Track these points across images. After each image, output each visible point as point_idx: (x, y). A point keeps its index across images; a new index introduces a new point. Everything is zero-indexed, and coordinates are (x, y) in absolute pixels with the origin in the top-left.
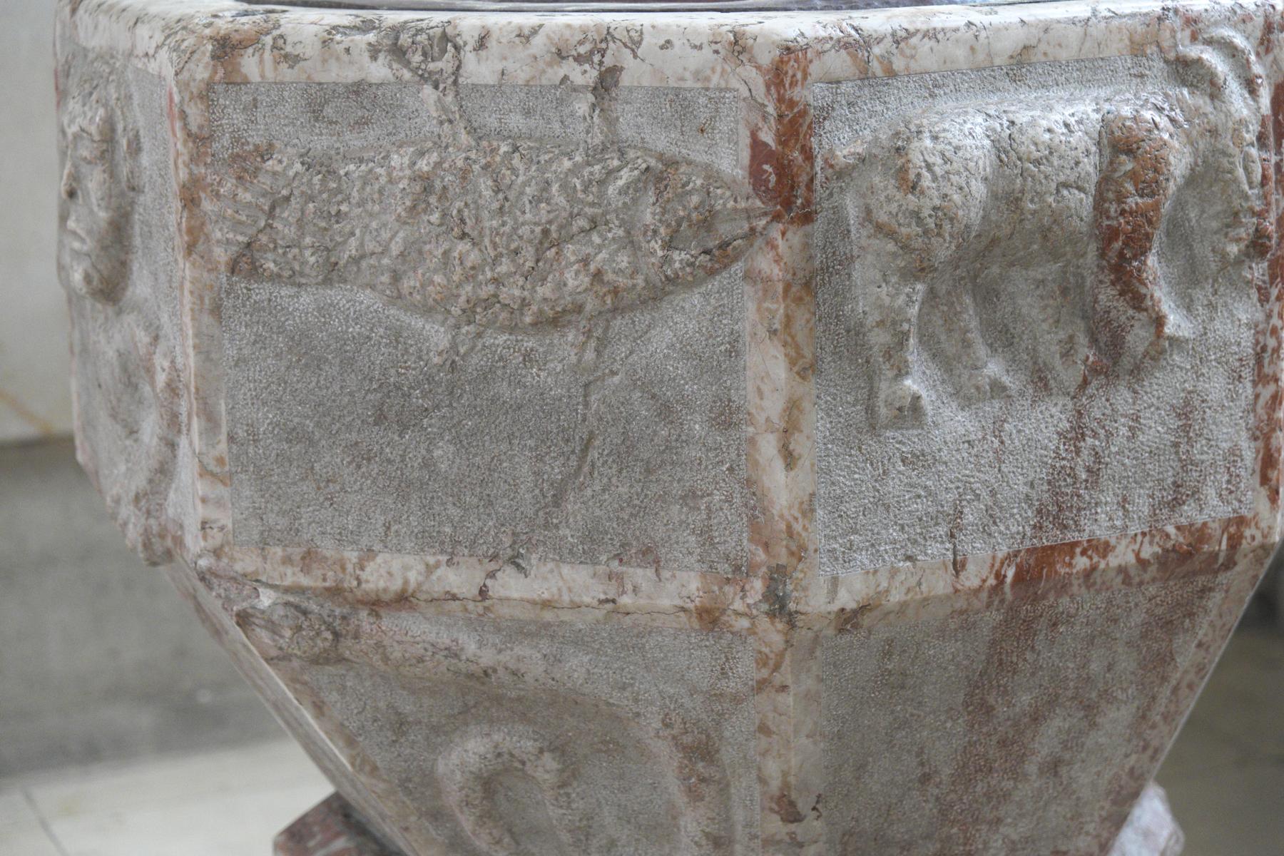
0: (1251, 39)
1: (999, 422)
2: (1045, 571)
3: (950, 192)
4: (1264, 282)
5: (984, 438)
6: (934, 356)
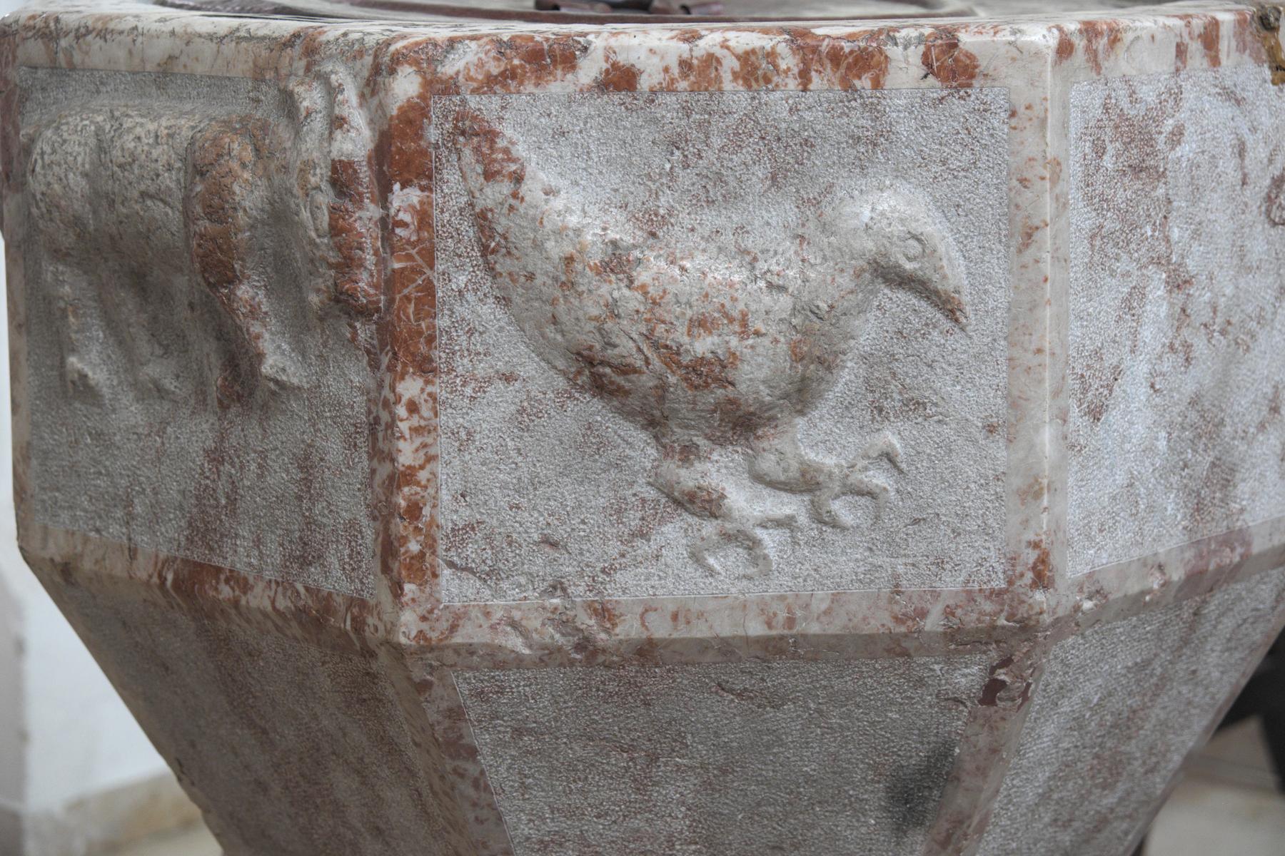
0: (359, 79)
1: (165, 423)
2: (197, 586)
3: (52, 181)
4: (373, 346)
5: (149, 435)
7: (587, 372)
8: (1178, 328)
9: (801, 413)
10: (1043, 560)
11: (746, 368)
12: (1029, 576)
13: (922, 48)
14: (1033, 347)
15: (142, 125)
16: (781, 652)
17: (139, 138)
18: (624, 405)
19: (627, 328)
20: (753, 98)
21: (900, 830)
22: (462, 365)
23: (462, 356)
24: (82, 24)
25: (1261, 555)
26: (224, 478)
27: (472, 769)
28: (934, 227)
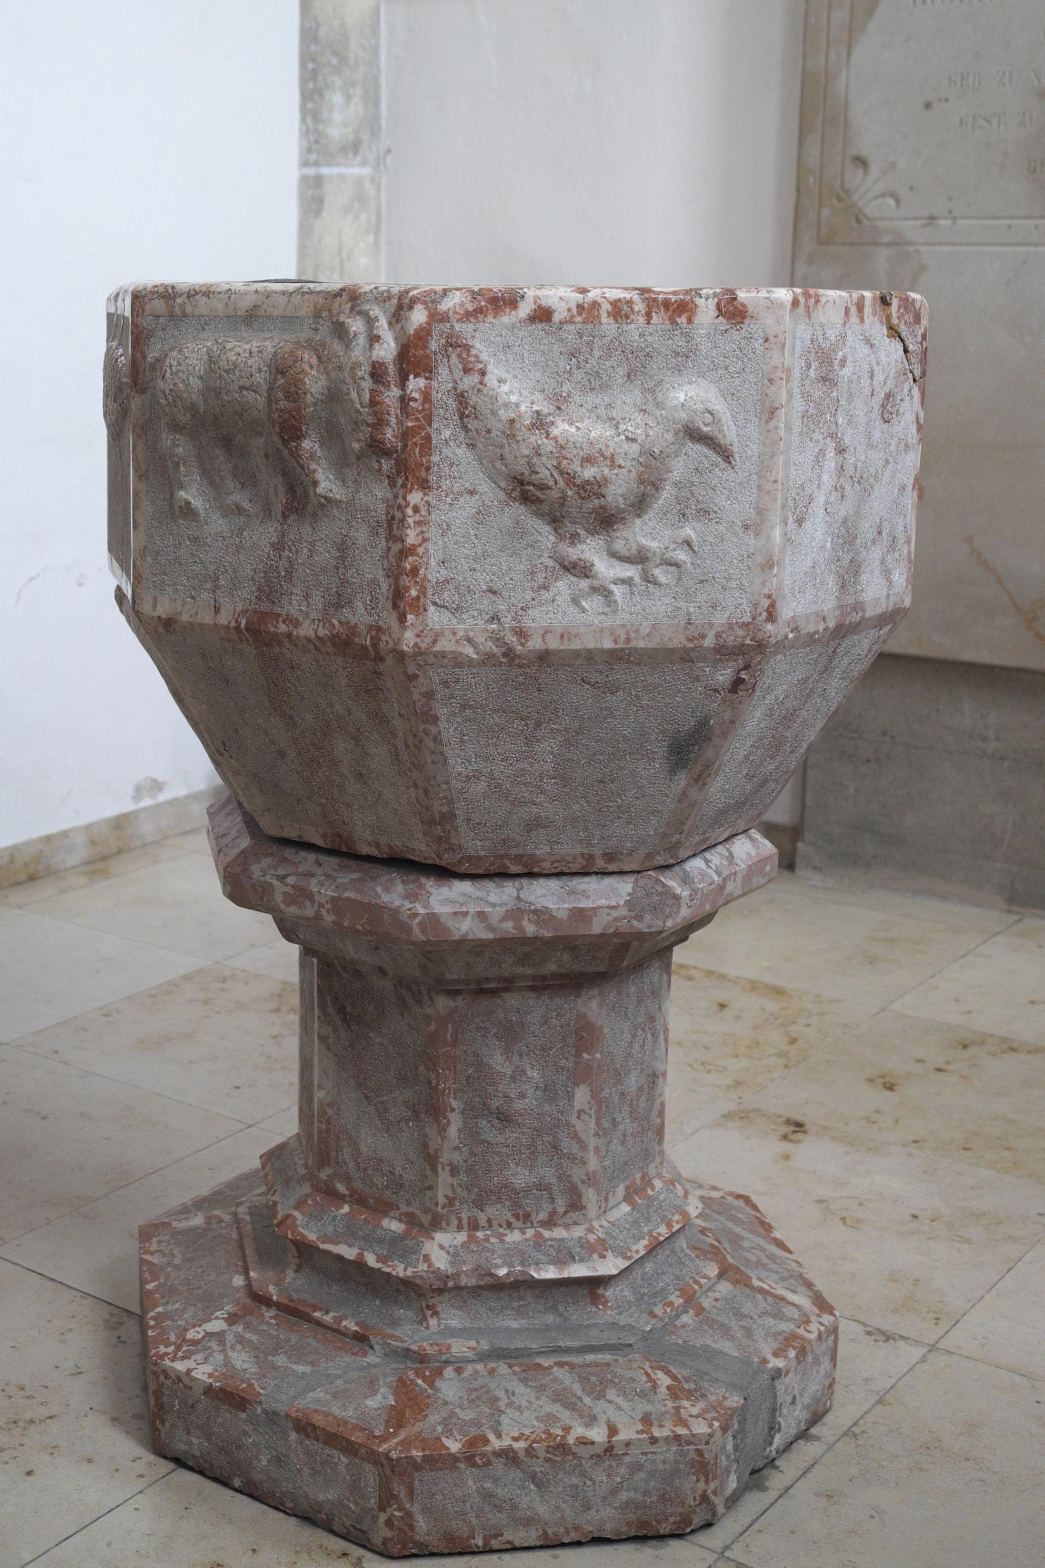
4: (392, 474)
6: (211, 483)
7: (518, 489)
8: (839, 477)
9: (639, 516)
10: (772, 605)
11: (613, 487)
12: (765, 614)
13: (716, 300)
14: (772, 479)
15: (239, 346)
16: (621, 658)
17: (239, 354)
18: (539, 509)
19: (545, 462)
20: (619, 328)
21: (673, 771)
22: (446, 484)
23: (445, 479)
24: (192, 288)
25: (871, 618)
26: (284, 559)
27: (433, 730)
28: (719, 406)
